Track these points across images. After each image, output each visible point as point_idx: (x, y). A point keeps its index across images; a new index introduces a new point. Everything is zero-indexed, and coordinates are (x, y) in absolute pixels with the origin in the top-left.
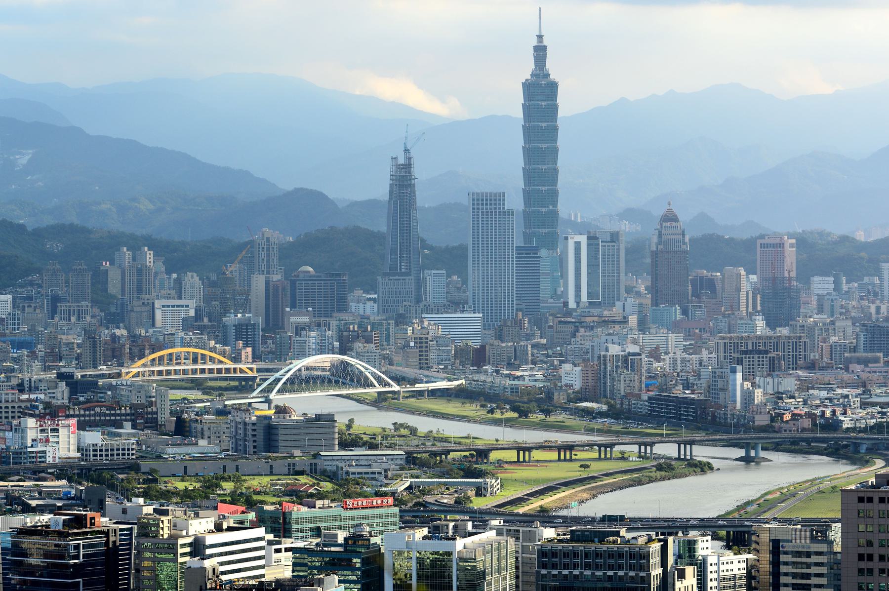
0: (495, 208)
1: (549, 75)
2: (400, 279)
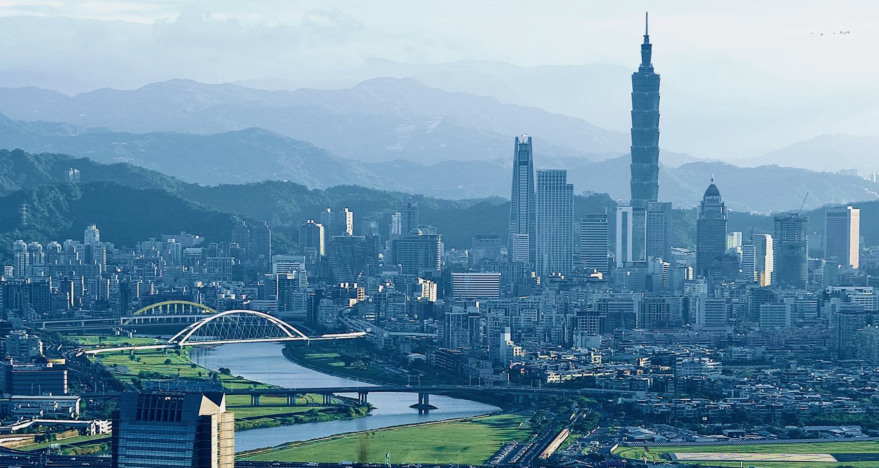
0: (561, 184)
2: (489, 241)
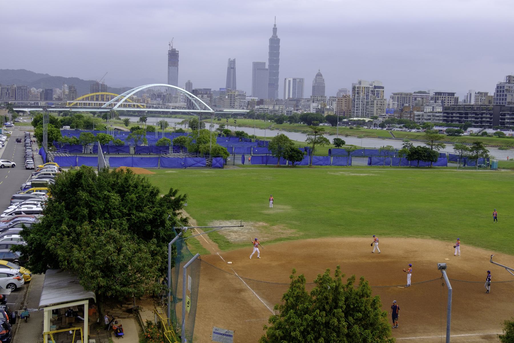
1: (277, 37)
